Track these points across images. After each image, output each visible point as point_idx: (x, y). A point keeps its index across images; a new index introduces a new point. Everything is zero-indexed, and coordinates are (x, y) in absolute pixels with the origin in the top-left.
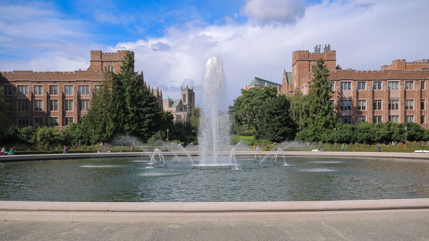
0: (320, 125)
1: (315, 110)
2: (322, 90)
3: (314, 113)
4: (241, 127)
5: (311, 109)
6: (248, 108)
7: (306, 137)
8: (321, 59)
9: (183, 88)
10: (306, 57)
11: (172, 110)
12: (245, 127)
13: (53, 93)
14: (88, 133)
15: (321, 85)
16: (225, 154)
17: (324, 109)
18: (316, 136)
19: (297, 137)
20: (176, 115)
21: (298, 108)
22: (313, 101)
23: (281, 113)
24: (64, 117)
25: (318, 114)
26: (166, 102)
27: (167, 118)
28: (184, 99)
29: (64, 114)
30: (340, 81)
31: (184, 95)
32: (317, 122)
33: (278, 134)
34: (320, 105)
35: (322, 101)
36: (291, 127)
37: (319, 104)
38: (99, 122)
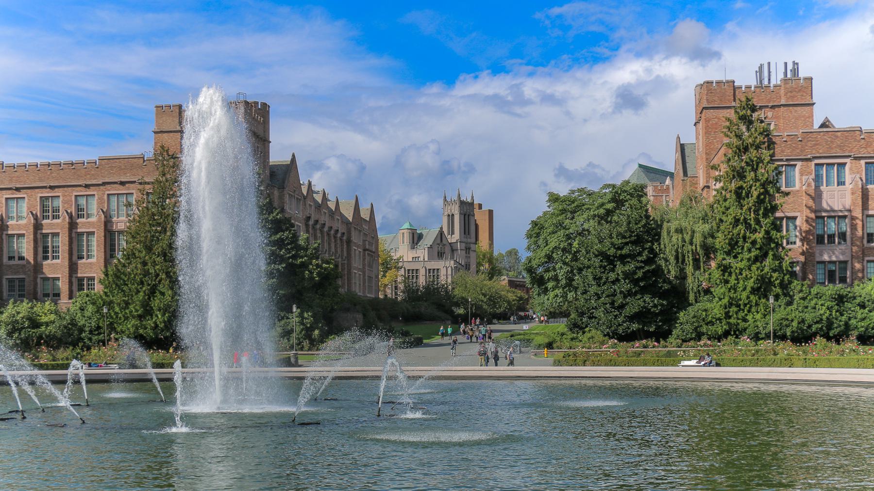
0: (745, 289)
1: (730, 244)
2: (751, 187)
3: (728, 253)
4: (546, 297)
5: (720, 241)
6: (560, 244)
7: (702, 323)
8: (748, 100)
9: (448, 199)
10: (728, 98)
11: (419, 257)
12: (554, 298)
13: (84, 214)
14: (112, 317)
15: (747, 174)
16: (434, 374)
17: (754, 243)
18: (732, 321)
19: (681, 324)
20: (426, 268)
21: (684, 241)
22: (725, 220)
23: (632, 256)
24: (74, 275)
25: (740, 256)
26: (403, 237)
27: (319, 274)
28: (449, 228)
29: (73, 268)
30: (813, 163)
31: (451, 217)
32: (737, 279)
33: (625, 316)
34: (742, 232)
35: (750, 219)
36: (663, 295)
37: (741, 228)
38: (139, 287)
